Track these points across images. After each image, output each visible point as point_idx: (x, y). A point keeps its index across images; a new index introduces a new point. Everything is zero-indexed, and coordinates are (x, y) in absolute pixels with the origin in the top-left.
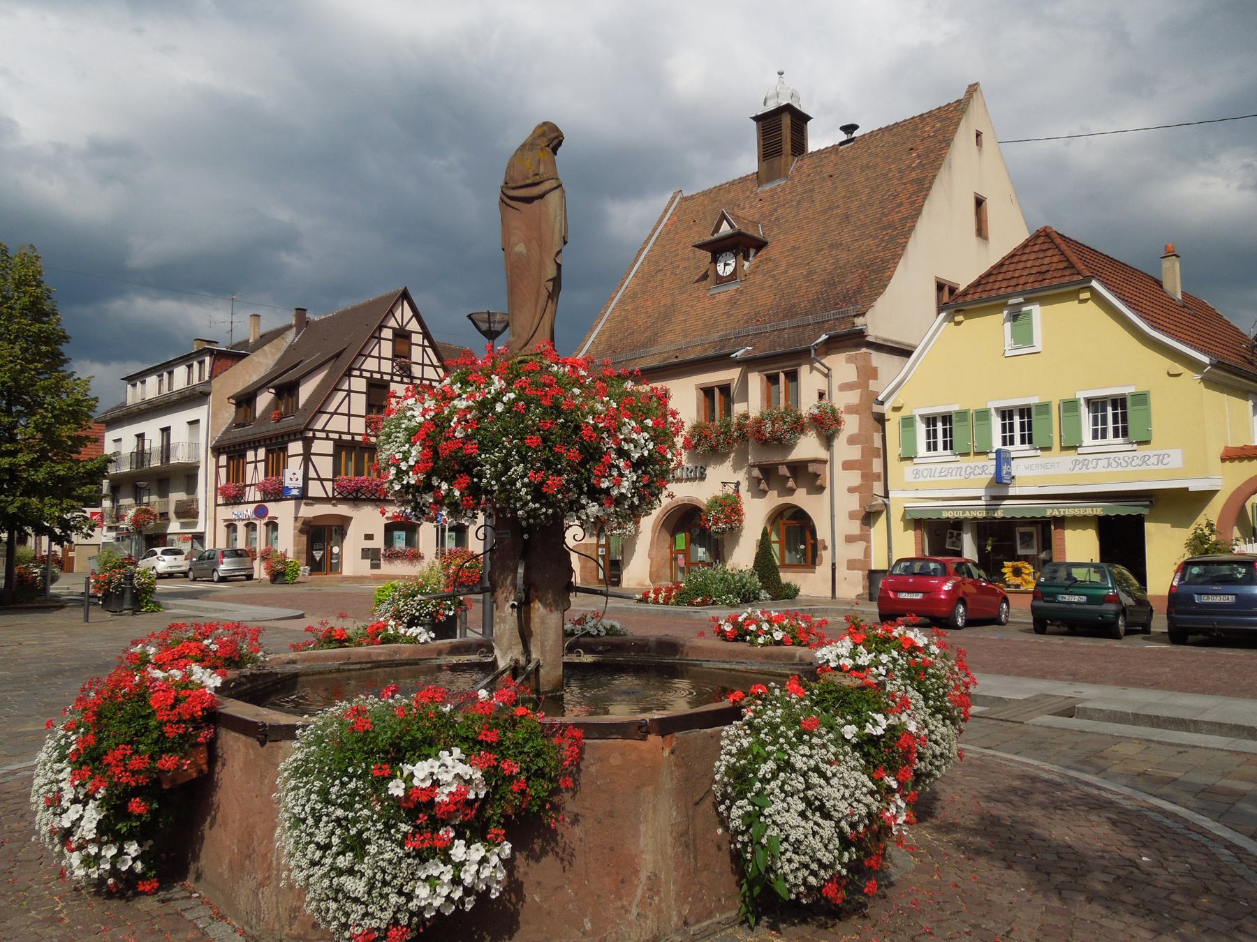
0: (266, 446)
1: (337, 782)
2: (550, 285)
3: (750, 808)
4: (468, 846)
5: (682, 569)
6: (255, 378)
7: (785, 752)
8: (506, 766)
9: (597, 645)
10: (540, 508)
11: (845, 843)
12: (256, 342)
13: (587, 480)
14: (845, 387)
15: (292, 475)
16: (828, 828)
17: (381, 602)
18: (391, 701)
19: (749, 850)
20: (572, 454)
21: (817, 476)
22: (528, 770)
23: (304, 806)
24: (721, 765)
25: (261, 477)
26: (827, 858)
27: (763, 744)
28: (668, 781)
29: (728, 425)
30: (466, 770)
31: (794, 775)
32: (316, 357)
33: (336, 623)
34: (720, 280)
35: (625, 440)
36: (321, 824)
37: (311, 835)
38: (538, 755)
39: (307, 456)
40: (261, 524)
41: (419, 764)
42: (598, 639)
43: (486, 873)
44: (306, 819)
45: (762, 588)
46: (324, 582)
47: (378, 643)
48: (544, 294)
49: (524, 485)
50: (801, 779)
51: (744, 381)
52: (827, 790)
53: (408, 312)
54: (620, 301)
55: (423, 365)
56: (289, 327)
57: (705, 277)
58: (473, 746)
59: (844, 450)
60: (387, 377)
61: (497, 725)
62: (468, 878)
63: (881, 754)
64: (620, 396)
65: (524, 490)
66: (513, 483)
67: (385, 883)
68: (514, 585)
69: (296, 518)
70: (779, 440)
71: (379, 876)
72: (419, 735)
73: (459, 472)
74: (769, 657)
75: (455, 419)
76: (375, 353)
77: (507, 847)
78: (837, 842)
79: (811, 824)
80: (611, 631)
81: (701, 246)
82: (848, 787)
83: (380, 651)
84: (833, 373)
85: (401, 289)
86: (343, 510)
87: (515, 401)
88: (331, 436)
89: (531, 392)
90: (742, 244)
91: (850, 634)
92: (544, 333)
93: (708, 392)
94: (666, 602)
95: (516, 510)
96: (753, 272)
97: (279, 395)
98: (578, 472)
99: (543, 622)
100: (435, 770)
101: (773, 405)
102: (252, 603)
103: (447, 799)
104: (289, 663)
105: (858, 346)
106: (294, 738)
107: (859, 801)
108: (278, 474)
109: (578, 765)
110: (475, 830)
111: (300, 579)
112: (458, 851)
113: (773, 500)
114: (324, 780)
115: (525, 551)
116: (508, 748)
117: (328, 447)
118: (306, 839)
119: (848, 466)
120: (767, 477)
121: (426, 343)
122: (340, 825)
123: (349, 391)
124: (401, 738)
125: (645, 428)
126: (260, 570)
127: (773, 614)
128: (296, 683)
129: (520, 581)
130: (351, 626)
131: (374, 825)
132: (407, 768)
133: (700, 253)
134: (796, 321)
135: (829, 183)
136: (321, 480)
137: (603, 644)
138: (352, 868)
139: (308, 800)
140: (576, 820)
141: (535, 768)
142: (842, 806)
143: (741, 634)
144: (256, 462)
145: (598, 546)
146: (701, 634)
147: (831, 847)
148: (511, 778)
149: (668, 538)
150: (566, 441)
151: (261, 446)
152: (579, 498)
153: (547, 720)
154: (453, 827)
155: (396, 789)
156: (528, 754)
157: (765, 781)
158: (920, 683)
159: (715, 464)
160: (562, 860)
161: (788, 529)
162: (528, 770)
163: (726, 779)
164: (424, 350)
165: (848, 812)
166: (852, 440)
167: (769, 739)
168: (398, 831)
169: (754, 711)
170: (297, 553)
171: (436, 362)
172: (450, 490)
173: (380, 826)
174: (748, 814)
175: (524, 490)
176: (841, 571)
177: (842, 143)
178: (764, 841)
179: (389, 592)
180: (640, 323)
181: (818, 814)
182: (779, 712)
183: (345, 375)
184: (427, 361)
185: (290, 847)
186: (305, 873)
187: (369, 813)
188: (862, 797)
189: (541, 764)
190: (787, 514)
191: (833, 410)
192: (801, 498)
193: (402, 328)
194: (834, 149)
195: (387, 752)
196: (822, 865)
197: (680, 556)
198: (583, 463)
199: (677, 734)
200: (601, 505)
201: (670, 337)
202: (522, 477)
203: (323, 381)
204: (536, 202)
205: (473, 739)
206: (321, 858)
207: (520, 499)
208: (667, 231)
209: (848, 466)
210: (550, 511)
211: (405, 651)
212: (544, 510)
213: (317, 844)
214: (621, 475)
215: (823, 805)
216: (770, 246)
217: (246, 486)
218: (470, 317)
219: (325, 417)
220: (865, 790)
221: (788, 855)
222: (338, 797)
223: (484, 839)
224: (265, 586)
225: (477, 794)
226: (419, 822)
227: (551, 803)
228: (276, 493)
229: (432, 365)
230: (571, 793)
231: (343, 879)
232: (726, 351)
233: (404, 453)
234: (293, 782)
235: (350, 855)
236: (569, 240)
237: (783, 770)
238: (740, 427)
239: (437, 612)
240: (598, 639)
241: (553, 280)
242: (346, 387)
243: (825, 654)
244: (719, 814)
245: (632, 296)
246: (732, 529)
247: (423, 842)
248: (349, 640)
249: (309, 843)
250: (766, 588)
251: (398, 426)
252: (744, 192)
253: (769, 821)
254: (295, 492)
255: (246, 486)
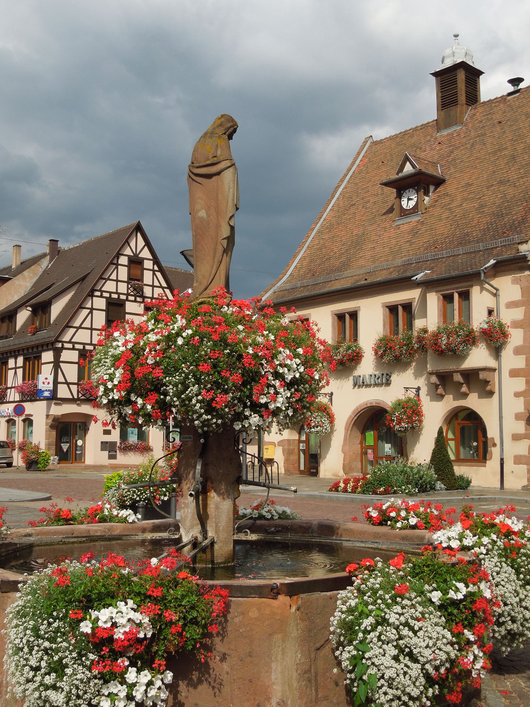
0: (24, 355)
1: (45, 622)
2: (225, 242)
3: (355, 653)
4: (139, 671)
5: (371, 463)
6: (16, 298)
7: (382, 610)
8: (167, 614)
9: (270, 526)
10: (212, 419)
11: (430, 681)
12: (17, 267)
13: (250, 397)
14: (511, 305)
15: (45, 379)
16: (415, 669)
17: (109, 488)
18: (88, 565)
19: (356, 684)
20: (235, 378)
21: (487, 382)
22: (185, 618)
23: (22, 638)
24: (334, 620)
25: (20, 381)
26: (415, 693)
27: (367, 604)
28: (295, 631)
29: (410, 338)
30: (137, 617)
31: (388, 628)
32: (66, 280)
33: (63, 505)
34: (404, 213)
35: (280, 365)
36: (34, 652)
37: (27, 660)
38: (193, 608)
39: (57, 364)
40: (19, 420)
41: (103, 611)
42: (272, 522)
43: (152, 692)
44: (23, 648)
45: (438, 480)
46: (70, 470)
47: (96, 522)
48: (220, 250)
49: (198, 401)
50: (394, 631)
51: (423, 300)
52: (415, 640)
53: (141, 242)
54: (319, 232)
55: (153, 286)
56: (44, 256)
57: (391, 210)
58: (143, 599)
59: (510, 360)
60: (123, 297)
61: (162, 585)
62: (138, 695)
63: (461, 615)
64: (278, 329)
65: (198, 405)
66: (190, 400)
67: (78, 697)
68: (194, 478)
69: (48, 416)
70: (454, 351)
71: (74, 691)
72: (103, 590)
73: (152, 391)
74: (404, 538)
75: (147, 350)
76: (114, 277)
77: (169, 676)
78: (422, 680)
79: (402, 666)
80: (283, 516)
81: (387, 184)
82: (433, 639)
83: (97, 528)
84: (501, 293)
85: (135, 222)
86: (86, 409)
87: (192, 336)
88: (77, 346)
89: (206, 330)
90: (422, 182)
91: (462, 521)
92: (220, 281)
93: (392, 309)
94: (354, 491)
95: (193, 420)
96: (432, 206)
97: (34, 312)
98: (241, 391)
99: (217, 508)
100: (114, 615)
101: (448, 321)
102: (10, 487)
103: (123, 637)
104: (26, 536)
105: (522, 269)
106: (18, 590)
107: (440, 649)
108: (33, 379)
109: (225, 616)
110: (144, 659)
111: (50, 467)
112: (131, 675)
113: (449, 403)
114: (36, 621)
115: (203, 453)
116: (170, 602)
117: (74, 356)
118: (24, 662)
119: (514, 373)
120: (444, 383)
121: (156, 268)
122: (47, 654)
123: (92, 309)
124: (91, 592)
125: (297, 356)
126: (18, 459)
127: (411, 503)
128: (31, 552)
129: (198, 475)
130: (78, 507)
131: (71, 654)
132: (94, 614)
133: (387, 189)
134: (468, 248)
135: (498, 129)
136: (68, 384)
137: (276, 526)
138: (55, 684)
139: (25, 635)
140: (224, 658)
141: (190, 617)
142: (427, 653)
143: (384, 520)
144: (16, 368)
145: (300, 441)
146: (354, 519)
147: (417, 684)
148: (171, 623)
149: (359, 435)
150: (231, 367)
151: (20, 355)
152: (243, 410)
153: (200, 582)
154: (128, 658)
155: (86, 627)
156: (185, 606)
157: (366, 632)
158: (513, 561)
159: (399, 371)
160: (213, 688)
161: (463, 429)
162: (185, 618)
163: (338, 631)
164: (154, 274)
165: (431, 657)
166: (517, 351)
167: (370, 600)
168: (87, 659)
169: (362, 579)
170: (48, 445)
171: (164, 284)
172: (144, 404)
173: (74, 655)
174: (354, 657)
175: (198, 405)
176: (509, 466)
177: (510, 94)
178: (365, 677)
179: (116, 480)
180: (336, 250)
181: (407, 658)
182: (379, 580)
183: (88, 295)
184: (156, 283)
185: (13, 669)
186: (23, 687)
187: (67, 645)
188: (442, 647)
189: (195, 614)
190: (462, 415)
191: (501, 325)
192: (473, 402)
193: (136, 255)
194: (503, 98)
195: (80, 602)
196: (411, 698)
197: (370, 451)
198: (244, 384)
199: (302, 596)
200: (261, 416)
201: (362, 262)
202: (197, 395)
203: (71, 300)
204: (214, 178)
205: (144, 594)
206: (34, 677)
207: (195, 412)
208: (359, 171)
209: (514, 373)
210: (220, 421)
211: (117, 528)
212: (215, 420)
213: (31, 667)
214: (277, 393)
215: (411, 651)
216: (447, 183)
217: (7, 388)
218: (182, 253)
219: (72, 331)
220: (445, 641)
221: (384, 689)
222: (46, 633)
223: (151, 669)
224: (22, 472)
225: (145, 635)
226: (103, 653)
227: (201, 643)
228: (32, 394)
229: (161, 287)
230: (220, 638)
231: (49, 692)
232: (408, 274)
233: (110, 375)
234: (15, 622)
235: (53, 675)
236: (239, 206)
237: (382, 625)
238: (420, 339)
239: (154, 497)
240: (272, 522)
241: (228, 238)
242: (89, 305)
243: (440, 536)
244: (336, 658)
245: (329, 227)
246: (413, 428)
247: (104, 667)
248: (74, 519)
249: (24, 666)
250: (442, 480)
251: (106, 353)
252: (425, 136)
253: (369, 663)
254: (47, 394)
255: (7, 388)
